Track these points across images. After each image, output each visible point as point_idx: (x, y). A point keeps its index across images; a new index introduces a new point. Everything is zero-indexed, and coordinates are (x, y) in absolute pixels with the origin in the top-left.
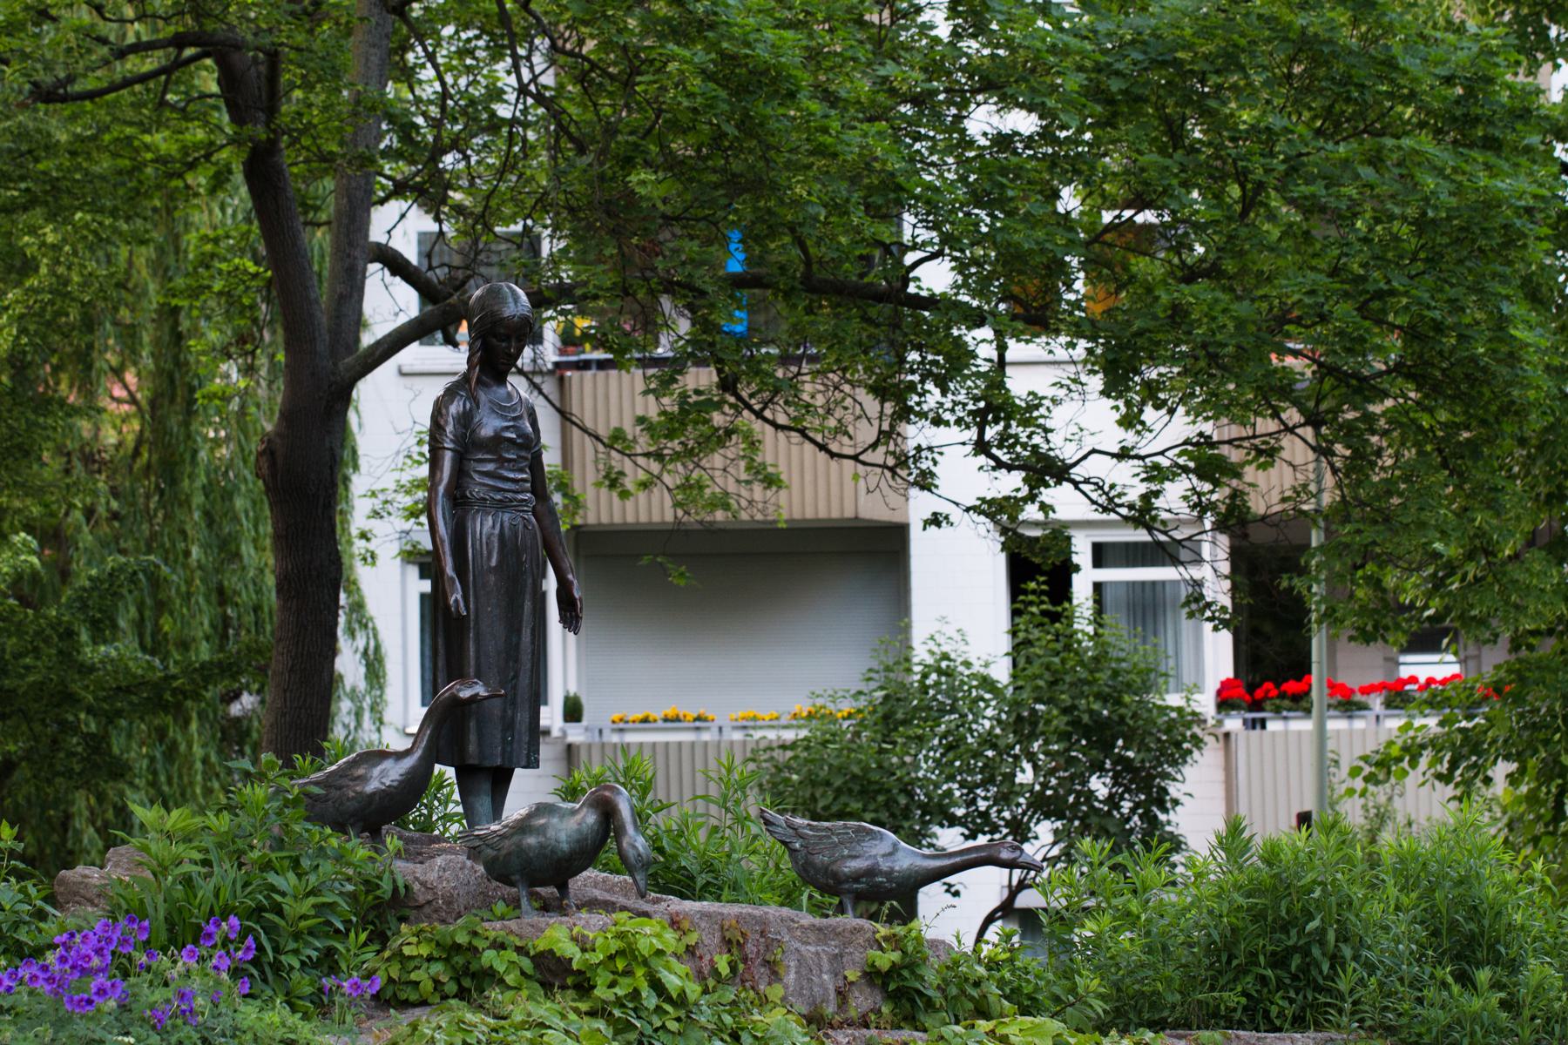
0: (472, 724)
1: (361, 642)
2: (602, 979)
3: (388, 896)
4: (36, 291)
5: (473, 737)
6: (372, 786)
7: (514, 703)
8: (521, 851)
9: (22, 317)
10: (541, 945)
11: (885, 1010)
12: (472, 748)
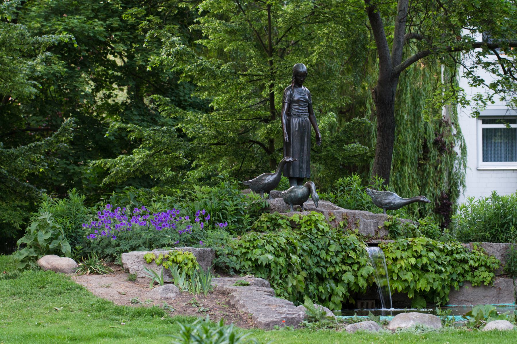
0: (291, 167)
1: (459, 143)
2: (303, 226)
3: (264, 207)
4: (322, 46)
5: (291, 170)
6: (266, 181)
7: (302, 162)
8: (290, 196)
9: (319, 53)
10: (291, 218)
11: (389, 235)
12: (291, 173)
